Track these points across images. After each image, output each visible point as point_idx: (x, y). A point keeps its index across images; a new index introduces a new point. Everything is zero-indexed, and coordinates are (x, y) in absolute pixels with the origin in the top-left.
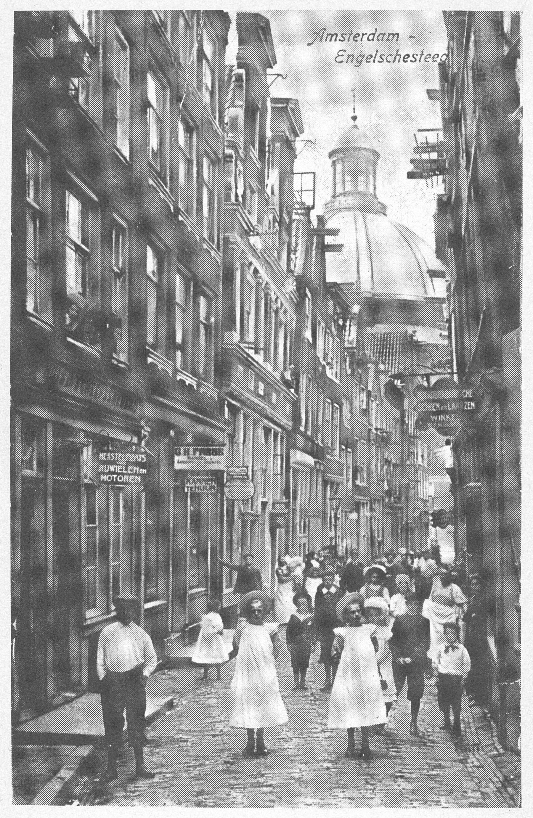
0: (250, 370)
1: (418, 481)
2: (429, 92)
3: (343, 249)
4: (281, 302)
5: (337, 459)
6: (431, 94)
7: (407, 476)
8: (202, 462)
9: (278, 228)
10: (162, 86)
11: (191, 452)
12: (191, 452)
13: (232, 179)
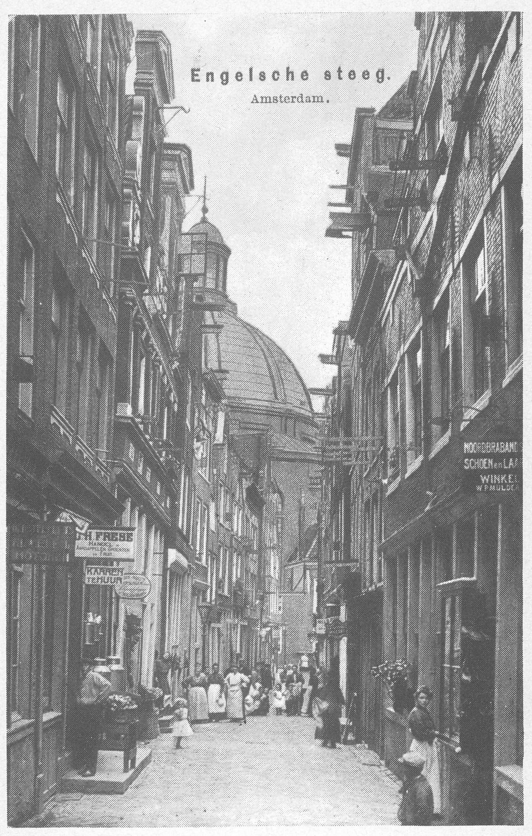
2: (339, 147)
5: (204, 564)
6: (341, 149)
8: (107, 548)
10: (68, 90)
11: (94, 536)
12: (94, 536)
13: (130, 223)
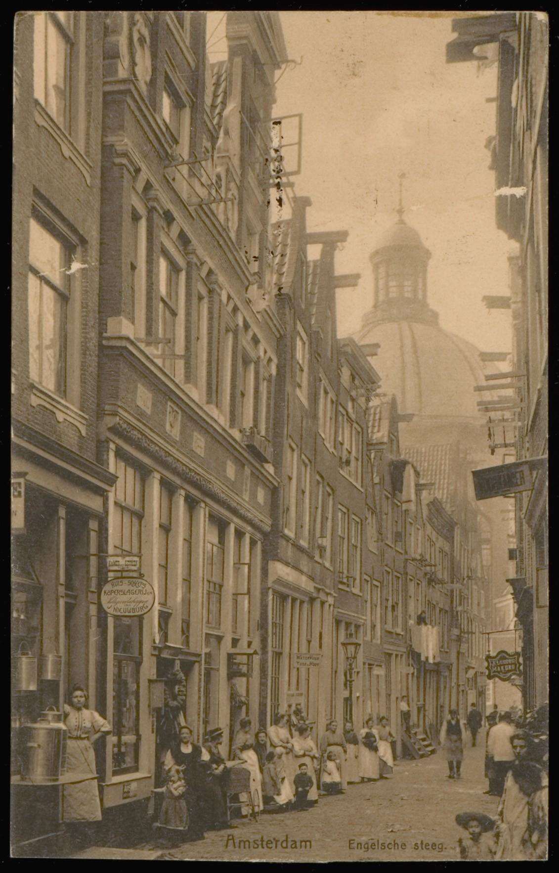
0: (169, 403)
1: (472, 633)
3: (360, 281)
4: (245, 321)
5: (356, 591)
7: (458, 626)
9: (236, 193)
